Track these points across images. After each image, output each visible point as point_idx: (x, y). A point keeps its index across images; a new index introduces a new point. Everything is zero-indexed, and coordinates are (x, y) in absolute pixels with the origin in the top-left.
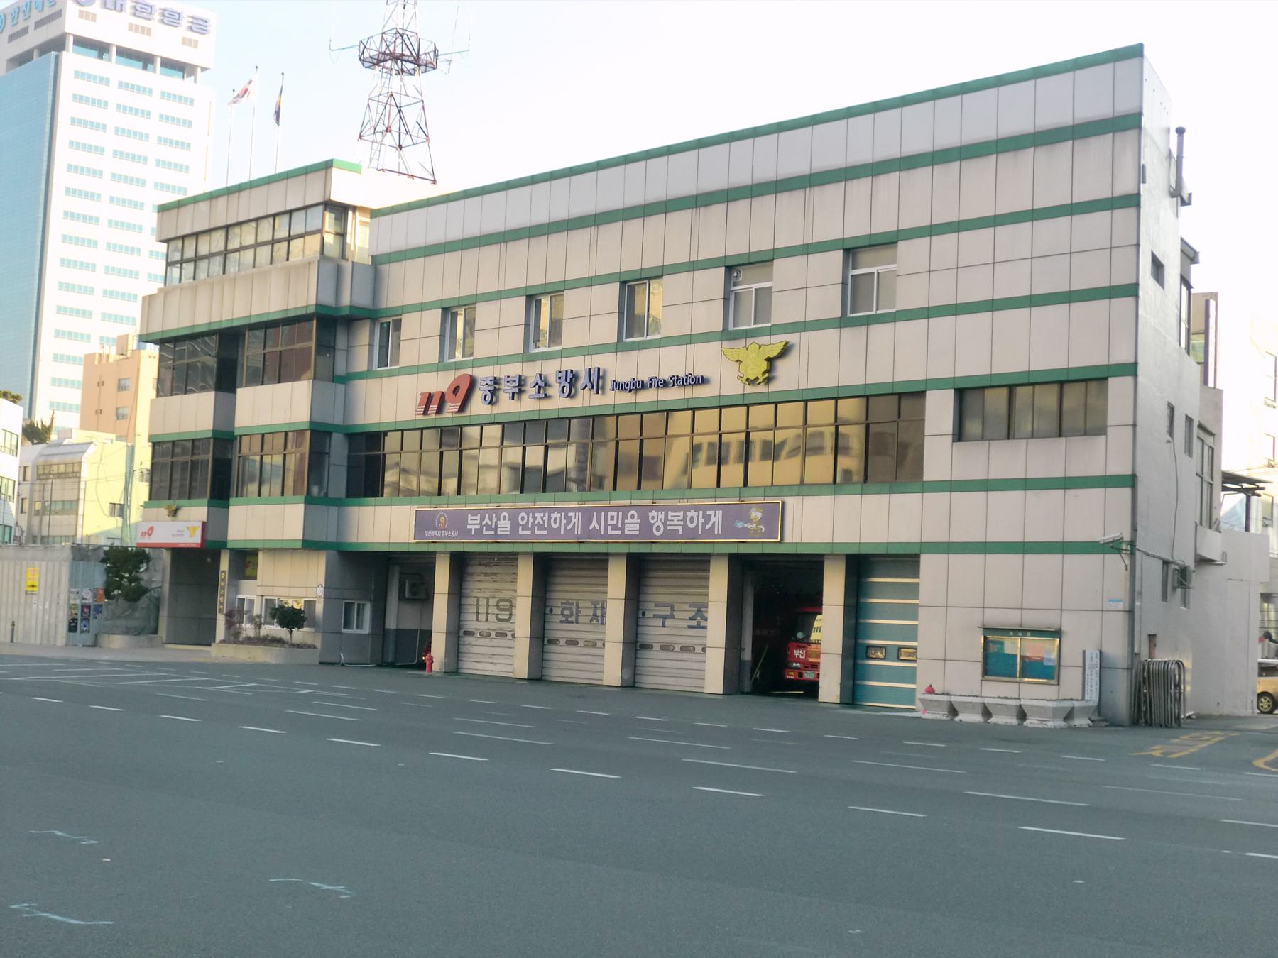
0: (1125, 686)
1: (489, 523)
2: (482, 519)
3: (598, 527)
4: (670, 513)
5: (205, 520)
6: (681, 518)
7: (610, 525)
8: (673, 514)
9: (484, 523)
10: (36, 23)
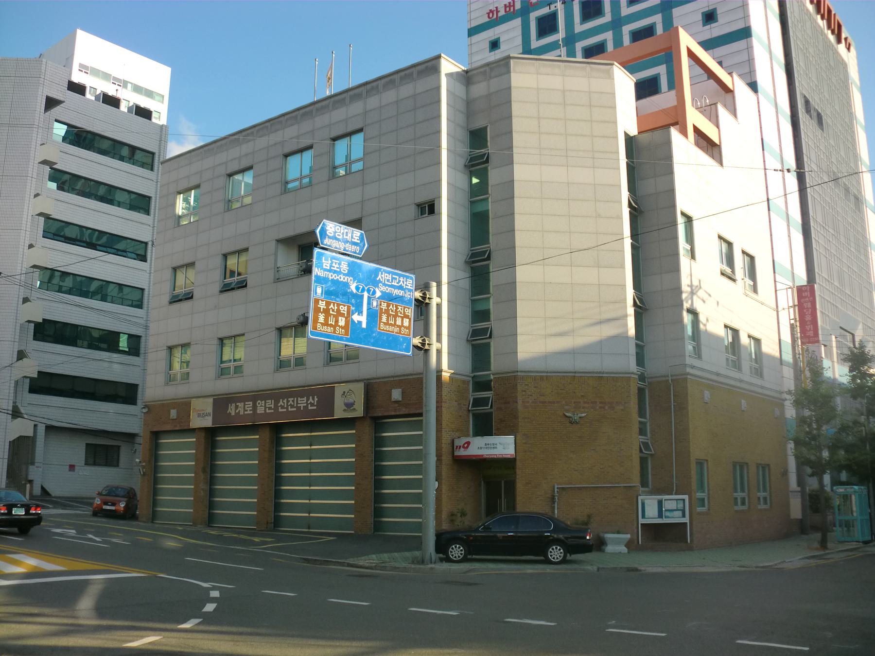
0: (355, 218)
1: (313, 402)
2: (308, 399)
3: (283, 404)
4: (299, 398)
5: (31, 467)
6: (267, 404)
7: (244, 413)
8: (301, 399)
9: (309, 402)
10: (34, 265)
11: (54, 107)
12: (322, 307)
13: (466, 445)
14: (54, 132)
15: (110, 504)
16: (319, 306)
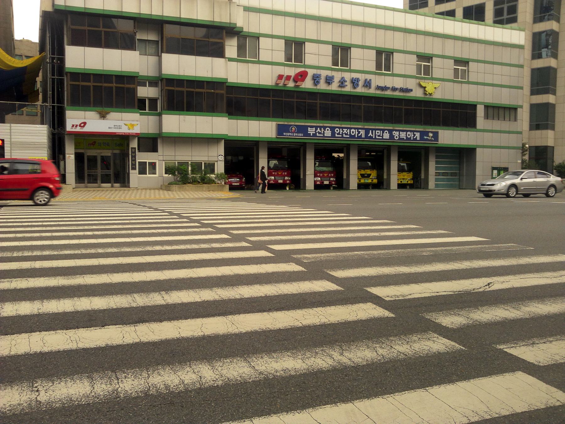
9: (317, 131)
11: (86, 107)
12: (312, 133)
13: (82, 125)
14: (164, 117)
15: (144, 92)
16: (309, 132)
